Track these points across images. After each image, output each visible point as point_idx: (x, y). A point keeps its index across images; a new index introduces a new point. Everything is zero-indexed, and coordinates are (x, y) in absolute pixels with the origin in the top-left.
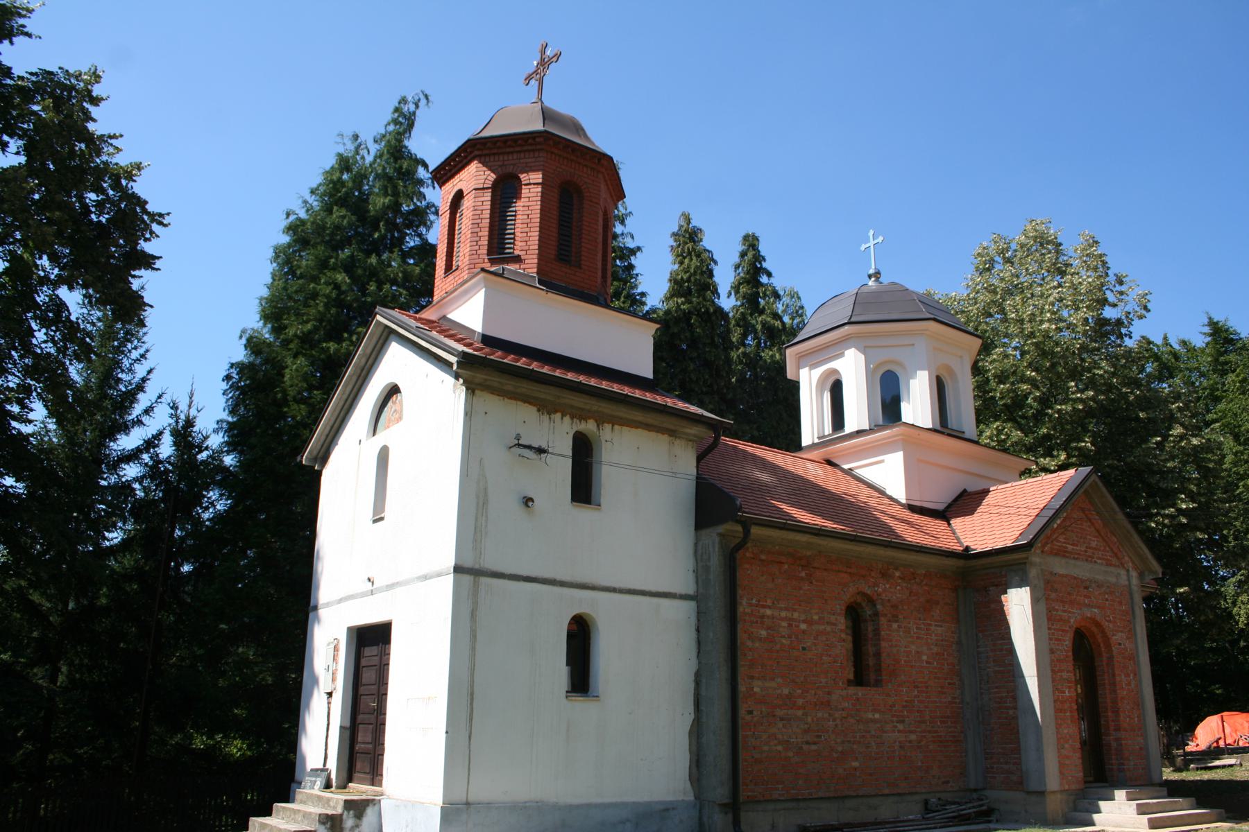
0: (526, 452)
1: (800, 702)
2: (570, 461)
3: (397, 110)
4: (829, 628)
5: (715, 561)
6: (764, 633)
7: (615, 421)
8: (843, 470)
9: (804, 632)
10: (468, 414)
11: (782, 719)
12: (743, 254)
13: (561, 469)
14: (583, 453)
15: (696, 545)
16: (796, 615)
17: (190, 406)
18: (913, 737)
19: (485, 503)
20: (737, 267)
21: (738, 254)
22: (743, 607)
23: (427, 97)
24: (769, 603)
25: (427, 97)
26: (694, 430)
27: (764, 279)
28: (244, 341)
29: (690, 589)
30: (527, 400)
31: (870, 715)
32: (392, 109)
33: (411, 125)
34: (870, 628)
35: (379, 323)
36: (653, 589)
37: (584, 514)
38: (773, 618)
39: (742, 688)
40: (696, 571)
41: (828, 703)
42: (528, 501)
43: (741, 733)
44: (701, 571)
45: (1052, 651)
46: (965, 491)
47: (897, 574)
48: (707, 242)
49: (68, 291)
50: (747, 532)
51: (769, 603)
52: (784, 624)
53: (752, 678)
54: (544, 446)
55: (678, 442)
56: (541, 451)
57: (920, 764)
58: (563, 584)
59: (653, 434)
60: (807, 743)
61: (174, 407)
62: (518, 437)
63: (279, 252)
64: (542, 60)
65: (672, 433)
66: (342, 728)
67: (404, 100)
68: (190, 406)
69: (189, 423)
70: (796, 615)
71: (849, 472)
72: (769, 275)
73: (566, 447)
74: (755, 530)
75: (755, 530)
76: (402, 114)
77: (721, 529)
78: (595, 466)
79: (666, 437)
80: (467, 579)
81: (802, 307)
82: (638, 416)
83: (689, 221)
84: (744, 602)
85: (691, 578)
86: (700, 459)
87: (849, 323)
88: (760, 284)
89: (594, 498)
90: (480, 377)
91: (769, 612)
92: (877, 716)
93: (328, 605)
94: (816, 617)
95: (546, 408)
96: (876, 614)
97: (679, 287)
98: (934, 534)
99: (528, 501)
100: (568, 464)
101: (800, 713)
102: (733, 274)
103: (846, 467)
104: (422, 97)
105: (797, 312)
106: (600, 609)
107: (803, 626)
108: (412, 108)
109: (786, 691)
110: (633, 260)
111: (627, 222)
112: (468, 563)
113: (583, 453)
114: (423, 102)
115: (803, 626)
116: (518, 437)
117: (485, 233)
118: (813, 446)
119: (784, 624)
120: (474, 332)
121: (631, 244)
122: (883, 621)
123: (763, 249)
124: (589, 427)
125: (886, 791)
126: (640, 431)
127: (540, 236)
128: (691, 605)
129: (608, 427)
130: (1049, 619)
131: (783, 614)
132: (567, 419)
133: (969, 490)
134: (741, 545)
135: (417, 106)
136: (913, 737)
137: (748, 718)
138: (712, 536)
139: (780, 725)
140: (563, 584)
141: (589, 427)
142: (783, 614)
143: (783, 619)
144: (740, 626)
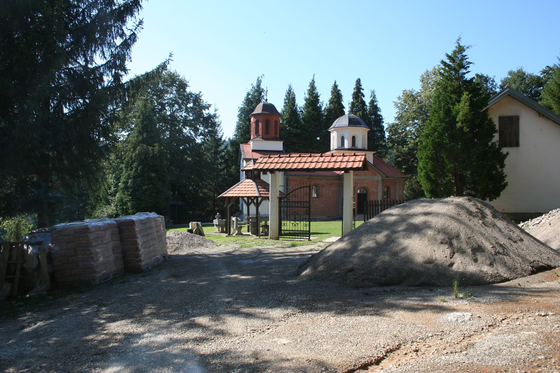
3: (258, 80)
18: (326, 206)
29: (283, 185)
72: (363, 89)
90: (247, 160)
122: (320, 188)
128: (283, 187)
136: (326, 206)
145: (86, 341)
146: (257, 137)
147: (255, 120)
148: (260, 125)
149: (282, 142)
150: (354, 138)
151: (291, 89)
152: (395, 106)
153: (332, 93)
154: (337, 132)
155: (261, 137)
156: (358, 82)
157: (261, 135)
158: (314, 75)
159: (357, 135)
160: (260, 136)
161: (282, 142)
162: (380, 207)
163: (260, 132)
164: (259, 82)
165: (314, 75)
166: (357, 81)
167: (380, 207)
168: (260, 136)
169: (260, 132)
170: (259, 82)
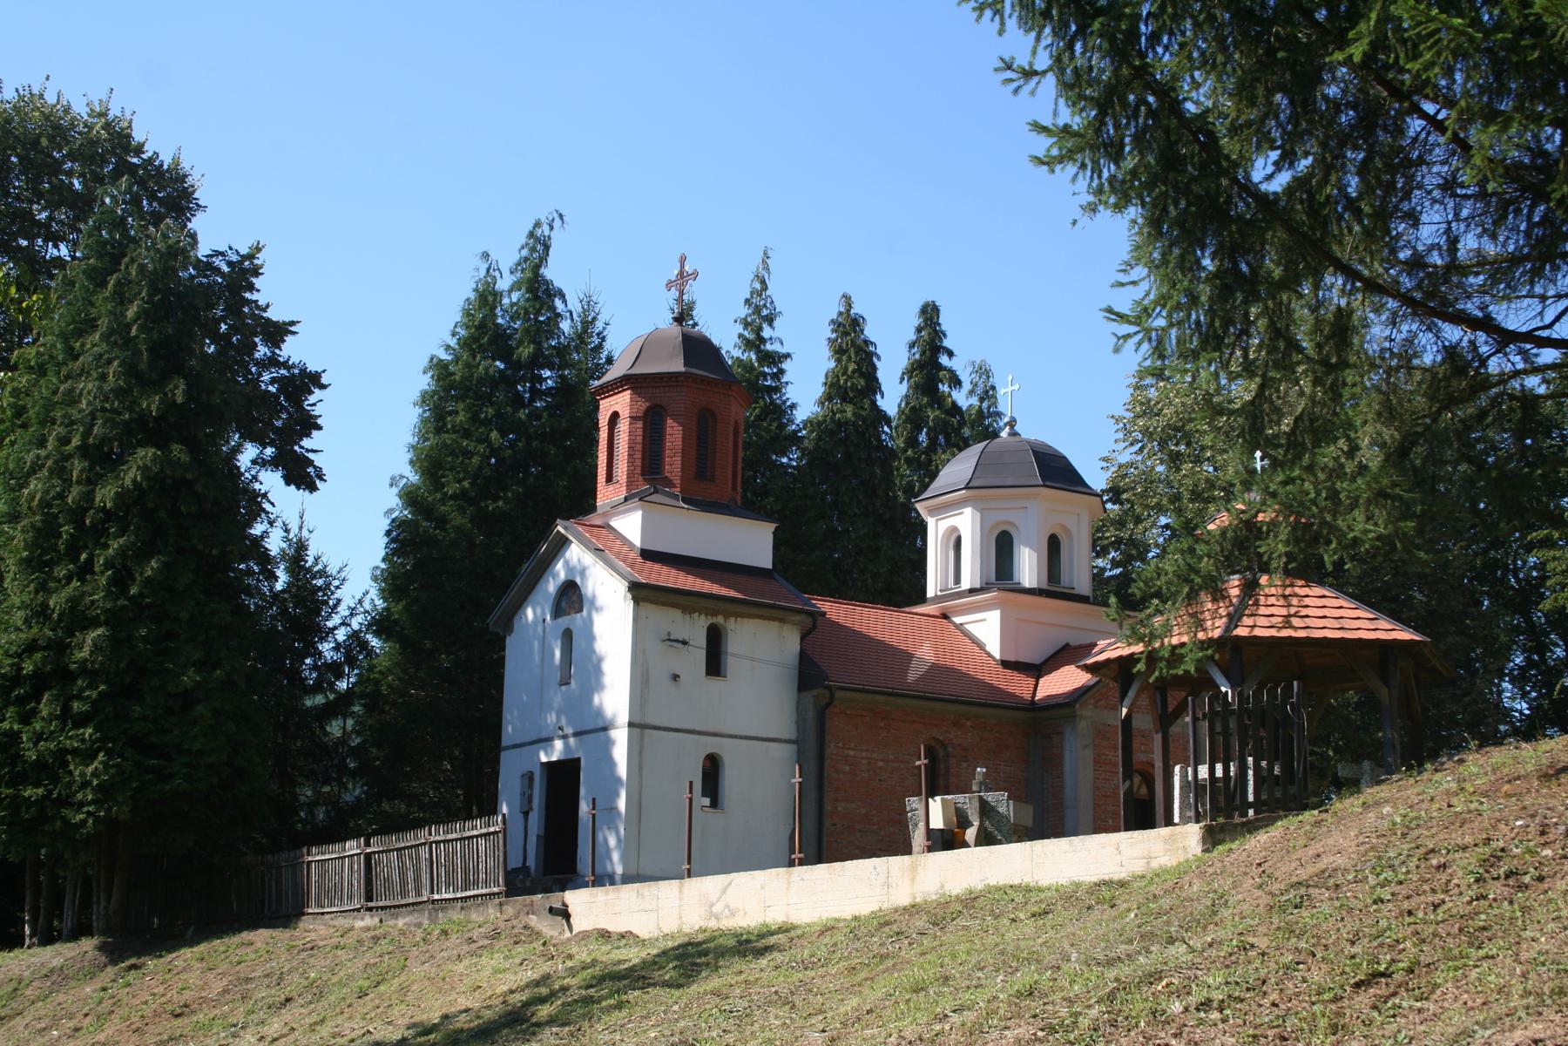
0: (675, 644)
1: (876, 819)
2: (704, 652)
3: (531, 235)
4: (902, 766)
5: (811, 714)
6: (847, 768)
7: (737, 615)
8: (954, 623)
9: (881, 768)
10: (635, 619)
12: (919, 330)
13: (697, 656)
14: (715, 640)
15: (798, 703)
16: (875, 755)
17: (301, 528)
19: (647, 679)
20: (912, 345)
21: (913, 330)
22: (831, 749)
23: (561, 216)
24: (852, 746)
25: (561, 216)
26: (797, 618)
27: (944, 360)
28: (395, 490)
29: (793, 736)
30: (673, 605)
32: (526, 233)
33: (547, 248)
34: (942, 766)
35: (558, 532)
36: (765, 736)
37: (715, 684)
39: (828, 807)
40: (797, 723)
42: (675, 677)
43: (825, 840)
44: (800, 723)
45: (1097, 788)
46: (1067, 645)
47: (969, 723)
48: (870, 332)
49: (282, 482)
50: (832, 694)
51: (852, 746)
52: (864, 762)
53: (836, 800)
54: (687, 638)
55: (785, 626)
56: (685, 643)
59: (766, 622)
61: (287, 531)
62: (669, 634)
63: (425, 398)
64: (681, 274)
65: (781, 620)
66: (538, 836)
67: (538, 224)
68: (301, 528)
69: (301, 547)
70: (875, 755)
71: (960, 627)
72: (951, 354)
73: (700, 639)
74: (839, 694)
75: (839, 694)
76: (538, 240)
77: (815, 693)
78: (723, 656)
79: (777, 624)
80: (636, 731)
81: (993, 388)
82: (754, 611)
83: (849, 306)
84: (832, 745)
85: (793, 727)
86: (802, 639)
87: (966, 488)
88: (940, 367)
89: (722, 673)
91: (852, 753)
93: (508, 748)
94: (891, 757)
95: (688, 610)
96: (948, 755)
97: (836, 390)
98: (1020, 686)
99: (675, 677)
100: (703, 653)
102: (907, 354)
103: (957, 620)
104: (556, 216)
105: (987, 392)
106: (730, 752)
107: (880, 764)
108: (546, 228)
109: (864, 811)
110: (784, 366)
111: (776, 323)
112: (637, 720)
113: (715, 640)
114: (557, 223)
115: (880, 764)
116: (669, 634)
117: (638, 455)
118: (937, 599)
119: (864, 762)
120: (634, 546)
121: (783, 350)
122: (953, 761)
123: (945, 322)
124: (720, 620)
126: (756, 620)
127: (683, 461)
128: (794, 747)
129: (732, 619)
130: (1096, 762)
131: (864, 754)
132: (703, 616)
133: (1072, 644)
134: (828, 705)
135: (552, 228)
137: (833, 828)
138: (809, 697)
141: (720, 620)
142: (864, 754)
144: (826, 764)
145: (822, 933)
146: (656, 491)
147: (643, 405)
148: (674, 433)
149: (772, 527)
150: (1054, 544)
151: (594, 319)
152: (1120, 435)
153: (839, 352)
154: (982, 511)
155: (677, 491)
156: (930, 314)
157: (677, 481)
158: (766, 256)
159: (1064, 528)
160: (673, 485)
161: (772, 527)
162: (1251, 798)
163: (673, 465)
164: (539, 246)
165: (766, 256)
166: (837, 325)
167: (1251, 798)
168: (671, 484)
169: (673, 465)
170: (539, 246)
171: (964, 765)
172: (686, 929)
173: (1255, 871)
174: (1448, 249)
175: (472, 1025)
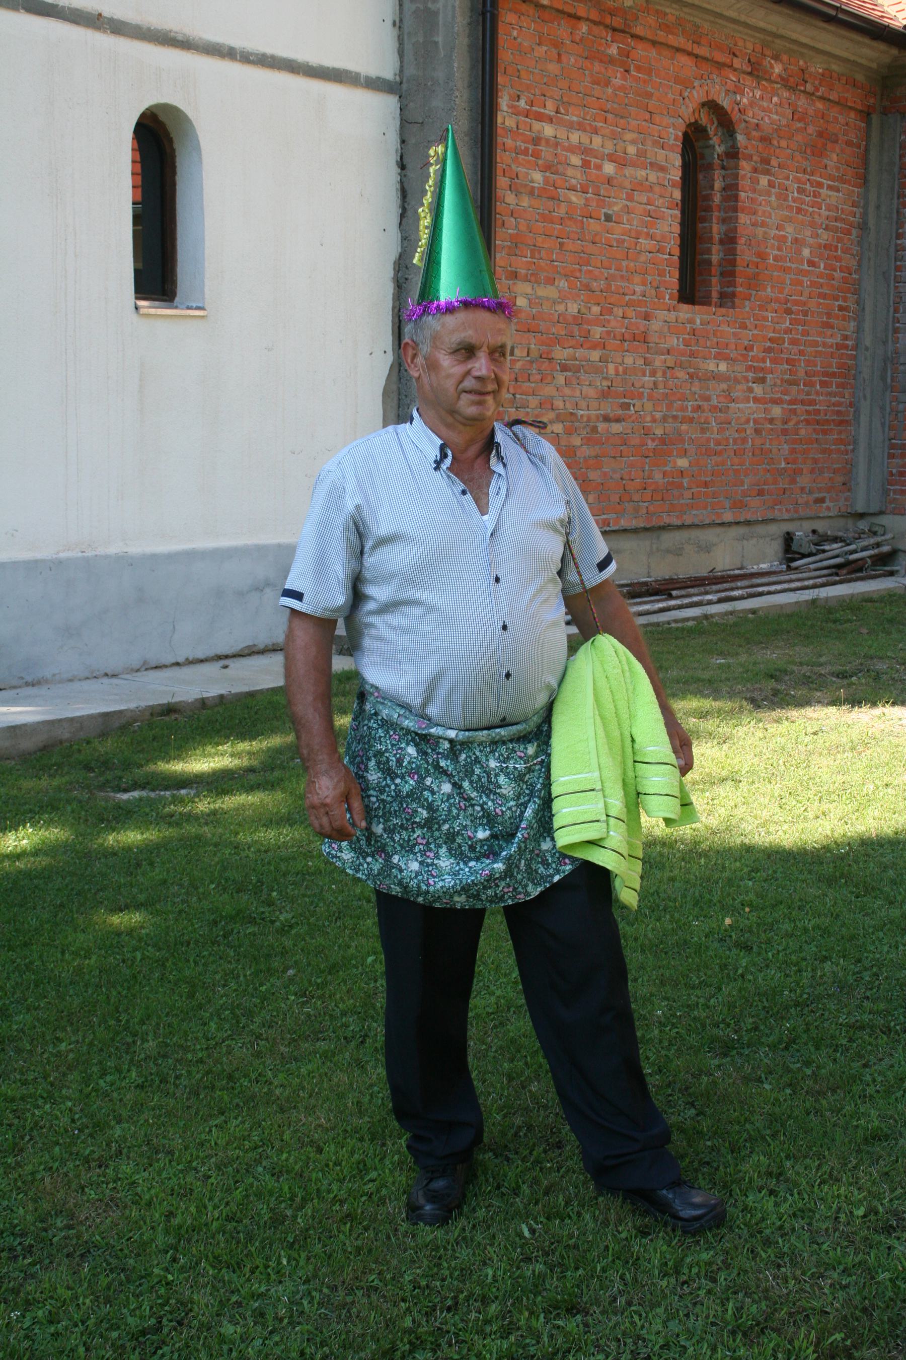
0: (77, 685)
1: (597, 332)
4: (653, 177)
6: (538, 177)
9: (609, 181)
11: (564, 368)
24: (550, 110)
29: (387, 70)
31: (711, 366)
36: (201, 656)
38: (557, 145)
41: (644, 338)
47: (778, 69)
51: (550, 110)
52: (576, 160)
57: (783, 465)
58: (118, 28)
60: (606, 419)
85: (387, 38)
91: (548, 131)
92: (723, 367)
101: (595, 355)
119: (576, 160)
125: (728, 517)
139: (560, 379)
140: (118, 28)
142: (575, 137)
143: (572, 149)
171: (764, 181)
172: (836, 835)
173: (768, 735)
174: (144, 1328)
175: (707, 704)
